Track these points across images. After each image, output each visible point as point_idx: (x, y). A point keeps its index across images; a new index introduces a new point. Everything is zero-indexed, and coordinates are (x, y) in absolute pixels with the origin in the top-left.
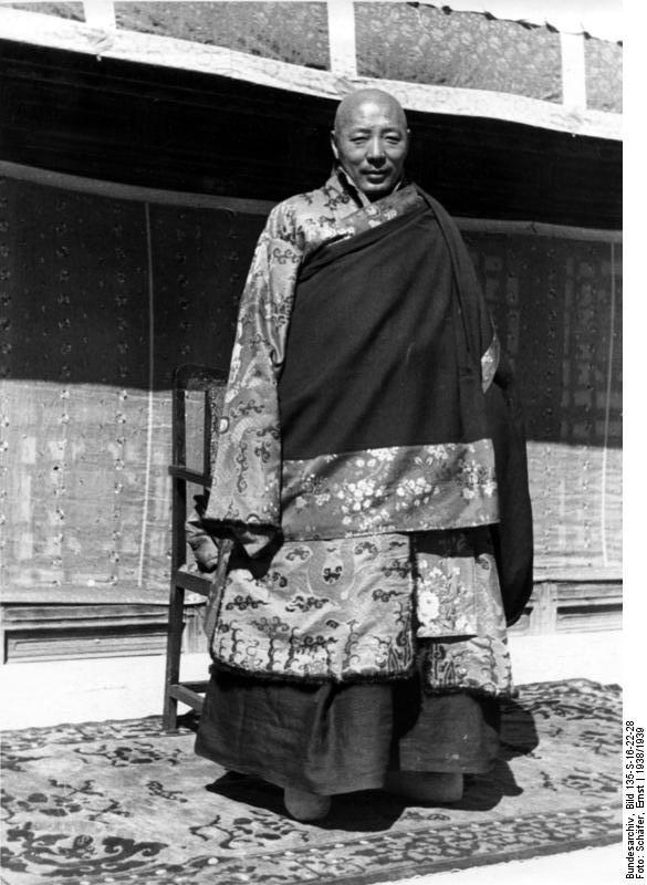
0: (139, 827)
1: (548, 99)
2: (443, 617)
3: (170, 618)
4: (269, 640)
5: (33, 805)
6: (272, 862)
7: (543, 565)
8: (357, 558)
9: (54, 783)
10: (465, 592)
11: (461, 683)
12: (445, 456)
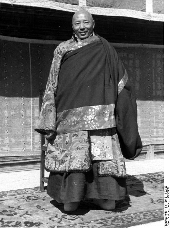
0: (34, 218)
1: (142, 11)
2: (102, 155)
3: (41, 159)
4: (55, 161)
5: (4, 213)
6: (73, 227)
7: (150, 140)
8: (73, 138)
9: (9, 207)
10: (109, 148)
11: (110, 173)
12: (98, 109)
